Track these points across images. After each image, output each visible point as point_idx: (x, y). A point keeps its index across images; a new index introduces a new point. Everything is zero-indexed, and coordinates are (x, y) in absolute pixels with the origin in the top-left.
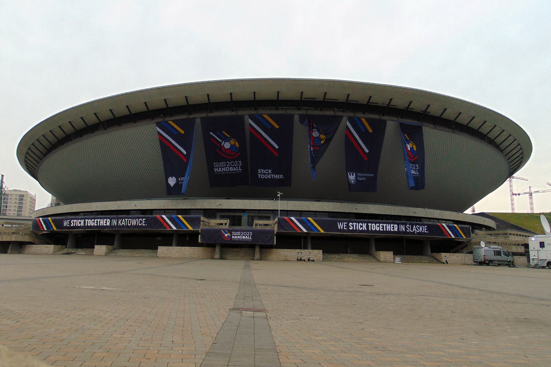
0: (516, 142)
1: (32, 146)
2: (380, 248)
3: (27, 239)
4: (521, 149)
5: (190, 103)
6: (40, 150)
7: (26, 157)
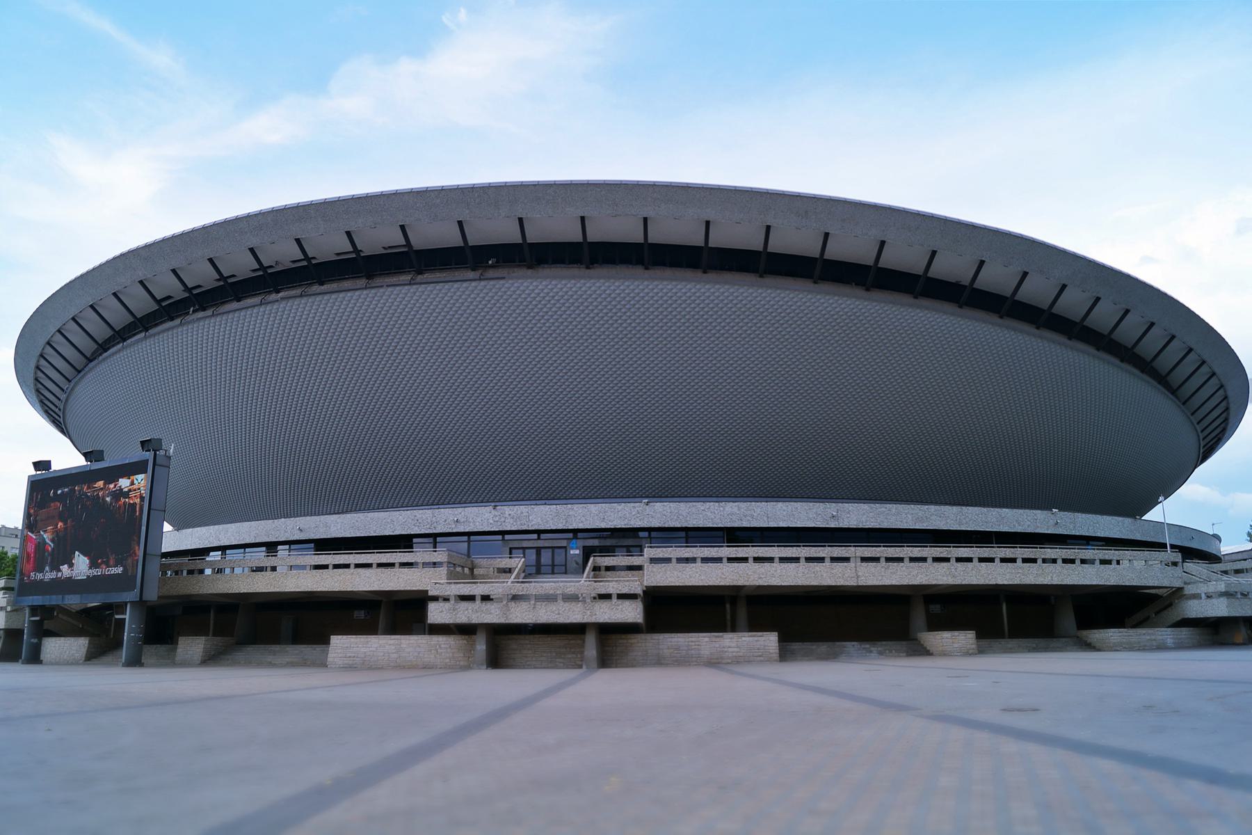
0: (1204, 369)
1: (49, 350)
2: (937, 624)
3: (632, 613)
4: (1226, 398)
5: (650, 241)
6: (71, 351)
7: (38, 368)
